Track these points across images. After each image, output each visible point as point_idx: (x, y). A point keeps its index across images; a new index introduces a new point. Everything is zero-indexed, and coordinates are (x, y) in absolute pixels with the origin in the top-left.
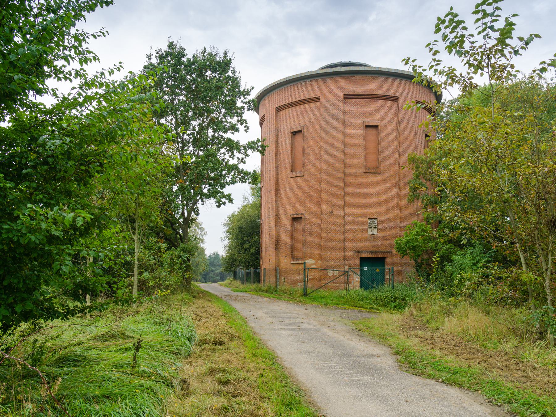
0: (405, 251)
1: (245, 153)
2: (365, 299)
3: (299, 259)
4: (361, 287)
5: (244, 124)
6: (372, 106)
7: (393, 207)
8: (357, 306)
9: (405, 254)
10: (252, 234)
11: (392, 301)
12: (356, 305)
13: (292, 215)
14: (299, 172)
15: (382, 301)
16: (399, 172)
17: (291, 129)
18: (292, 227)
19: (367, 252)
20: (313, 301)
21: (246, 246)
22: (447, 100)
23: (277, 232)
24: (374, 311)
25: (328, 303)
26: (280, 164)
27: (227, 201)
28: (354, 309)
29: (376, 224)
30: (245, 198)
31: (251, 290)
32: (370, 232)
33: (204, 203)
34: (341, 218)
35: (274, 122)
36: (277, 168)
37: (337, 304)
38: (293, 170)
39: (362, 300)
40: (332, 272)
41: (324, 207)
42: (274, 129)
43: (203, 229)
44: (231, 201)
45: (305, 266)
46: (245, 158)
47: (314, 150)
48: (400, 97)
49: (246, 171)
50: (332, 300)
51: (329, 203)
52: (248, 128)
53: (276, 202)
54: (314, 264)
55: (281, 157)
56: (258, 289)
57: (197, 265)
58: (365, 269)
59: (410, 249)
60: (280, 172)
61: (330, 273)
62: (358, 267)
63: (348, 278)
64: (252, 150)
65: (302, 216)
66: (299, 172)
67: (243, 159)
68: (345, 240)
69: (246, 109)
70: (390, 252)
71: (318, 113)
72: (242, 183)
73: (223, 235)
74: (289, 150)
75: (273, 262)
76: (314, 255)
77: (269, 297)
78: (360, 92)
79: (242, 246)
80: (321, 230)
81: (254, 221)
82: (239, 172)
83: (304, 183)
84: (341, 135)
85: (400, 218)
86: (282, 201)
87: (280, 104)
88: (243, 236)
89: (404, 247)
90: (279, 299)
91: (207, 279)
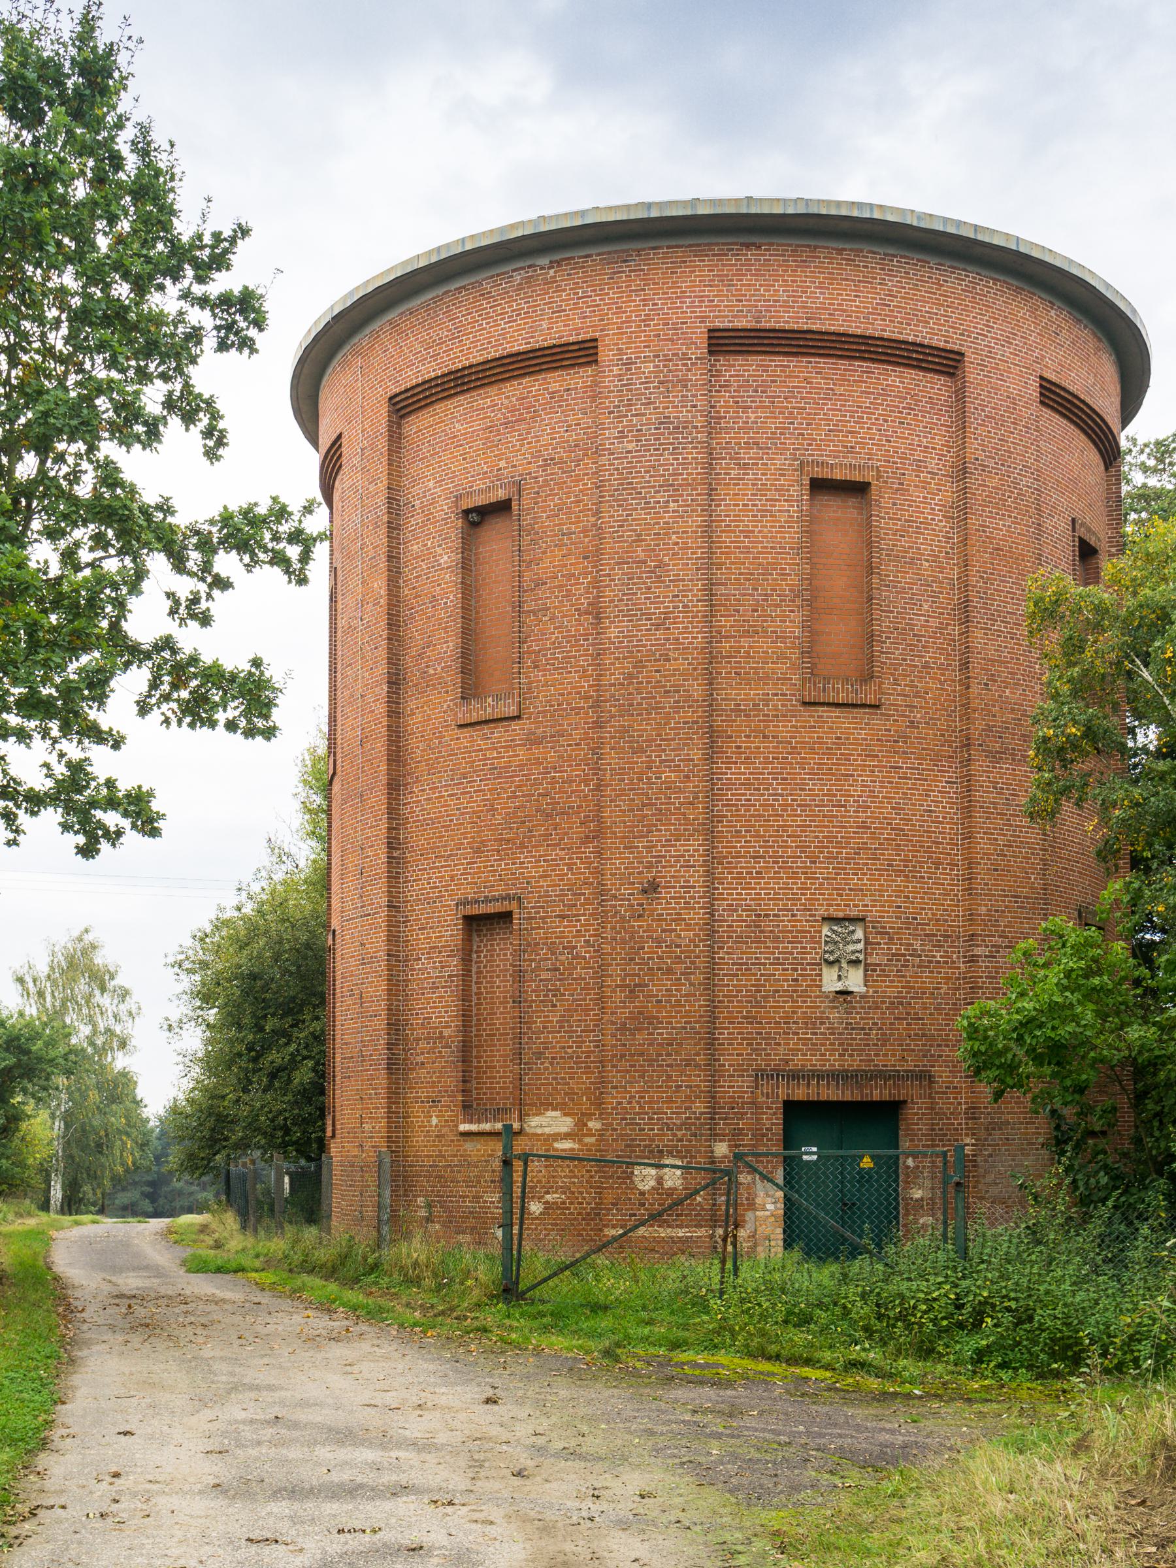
0: (1011, 1068)
1: (206, 567)
2: (822, 1316)
3: (497, 1114)
4: (788, 1244)
5: (204, 420)
6: (840, 390)
7: (937, 864)
8: (778, 1357)
9: (1009, 1081)
10: (302, 1006)
11: (961, 1326)
12: (773, 1349)
13: (466, 902)
14: (497, 698)
15: (909, 1326)
16: (966, 706)
17: (458, 498)
18: (466, 960)
19: (818, 1075)
20: (546, 1329)
21: (274, 1057)
22: (1140, 442)
23: (396, 985)
24: (874, 1384)
25: (627, 1337)
26: (409, 662)
27: (126, 823)
28: (765, 1380)
29: (860, 946)
30: (281, 855)
31: (269, 1263)
32: (830, 981)
33: (21, 838)
34: (697, 915)
35: (383, 468)
36: (395, 682)
37: (675, 1345)
38: (470, 690)
39: (805, 1320)
40: (653, 1172)
41: (618, 864)
42: (382, 500)
43: (124, 994)
44: (148, 824)
45: (508, 1148)
46: (209, 596)
47: (569, 594)
48: (968, 352)
49: (216, 665)
50: (651, 1322)
51: (641, 844)
52: (220, 443)
53: (393, 844)
54: (567, 1136)
55: (416, 632)
56: (297, 1258)
57: (99, 1146)
58: (810, 1154)
59: (1038, 1060)
60: (412, 703)
61: (645, 1178)
62: (777, 1149)
63: (732, 1202)
64: (247, 559)
65: (513, 906)
66: (497, 698)
67: (195, 600)
68: (712, 1016)
69: (210, 342)
70: (925, 1077)
71: (586, 421)
72: (192, 725)
73: (180, 1009)
74: (452, 598)
75: (377, 1126)
76: (571, 1093)
77: (327, 1307)
78: (784, 320)
79: (255, 1060)
80: (602, 972)
81: (308, 946)
82: (181, 670)
83: (520, 751)
84: (695, 520)
85: (971, 916)
86: (417, 838)
87: (411, 378)
88: (260, 1013)
89: (1007, 1049)
90: (375, 1315)
91: (161, 1201)
